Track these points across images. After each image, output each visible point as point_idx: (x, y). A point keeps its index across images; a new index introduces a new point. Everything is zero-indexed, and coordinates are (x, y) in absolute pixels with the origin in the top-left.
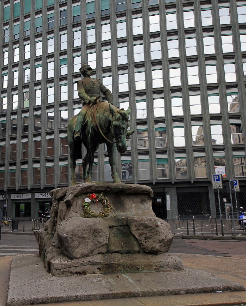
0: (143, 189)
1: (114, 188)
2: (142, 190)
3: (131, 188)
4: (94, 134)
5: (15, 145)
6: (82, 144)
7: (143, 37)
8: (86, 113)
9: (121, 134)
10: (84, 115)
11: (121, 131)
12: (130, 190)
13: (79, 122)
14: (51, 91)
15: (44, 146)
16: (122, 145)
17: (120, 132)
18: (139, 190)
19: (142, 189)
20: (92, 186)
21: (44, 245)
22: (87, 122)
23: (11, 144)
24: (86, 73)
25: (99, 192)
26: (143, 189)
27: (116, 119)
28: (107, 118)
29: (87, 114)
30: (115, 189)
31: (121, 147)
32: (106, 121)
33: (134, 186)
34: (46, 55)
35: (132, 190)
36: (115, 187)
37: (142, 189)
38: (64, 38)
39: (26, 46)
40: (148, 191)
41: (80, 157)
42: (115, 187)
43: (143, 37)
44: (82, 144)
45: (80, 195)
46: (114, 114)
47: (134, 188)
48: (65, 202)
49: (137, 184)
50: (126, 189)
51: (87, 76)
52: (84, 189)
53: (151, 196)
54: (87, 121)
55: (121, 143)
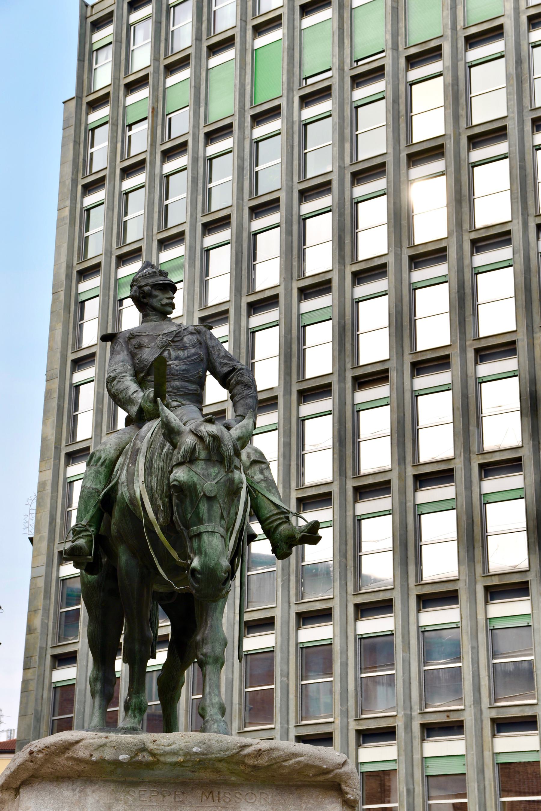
0: (302, 759)
1: (168, 749)
2: (299, 762)
3: (247, 751)
7: (509, 232)
12: (243, 763)
14: (376, 424)
15: (286, 669)
17: (197, 513)
18: (285, 764)
19: (299, 759)
20: (77, 742)
25: (140, 782)
26: (302, 759)
30: (174, 753)
31: (199, 573)
33: (258, 747)
34: (296, 285)
35: (251, 762)
36: (173, 747)
37: (299, 759)
38: (320, 231)
39: (211, 252)
40: (327, 772)
42: (173, 747)
43: (509, 232)
45: (25, 783)
47: (259, 753)
49: (300, 739)
50: (223, 755)
52: (41, 755)
53: (347, 793)
55: (200, 558)
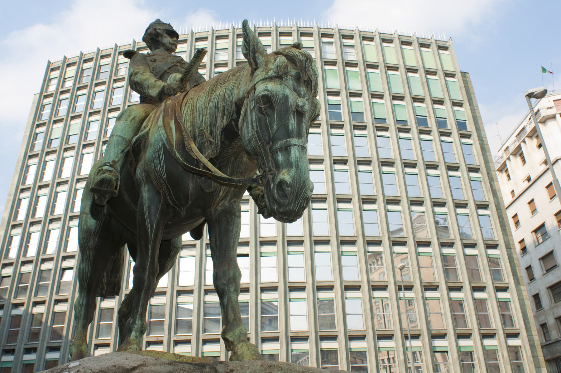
4: (165, 176)
5: (19, 317)
6: (126, 245)
8: (144, 115)
9: (289, 135)
10: (137, 120)
11: (287, 120)
13: (118, 140)
16: (293, 179)
21: (170, 364)
22: (146, 136)
23: (13, 316)
24: (160, 38)
27: (271, 73)
28: (227, 96)
29: (146, 120)
31: (288, 185)
32: (221, 109)
41: (113, 290)
44: (126, 245)
46: (261, 60)
48: (219, 339)
51: (161, 48)
54: (148, 133)
